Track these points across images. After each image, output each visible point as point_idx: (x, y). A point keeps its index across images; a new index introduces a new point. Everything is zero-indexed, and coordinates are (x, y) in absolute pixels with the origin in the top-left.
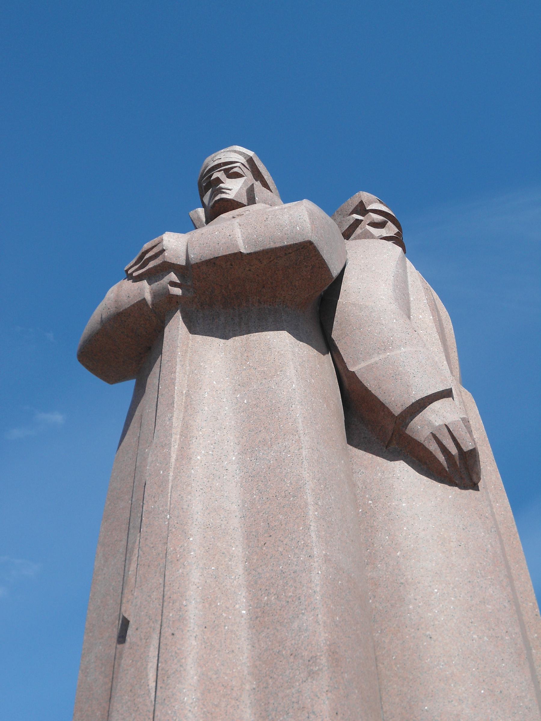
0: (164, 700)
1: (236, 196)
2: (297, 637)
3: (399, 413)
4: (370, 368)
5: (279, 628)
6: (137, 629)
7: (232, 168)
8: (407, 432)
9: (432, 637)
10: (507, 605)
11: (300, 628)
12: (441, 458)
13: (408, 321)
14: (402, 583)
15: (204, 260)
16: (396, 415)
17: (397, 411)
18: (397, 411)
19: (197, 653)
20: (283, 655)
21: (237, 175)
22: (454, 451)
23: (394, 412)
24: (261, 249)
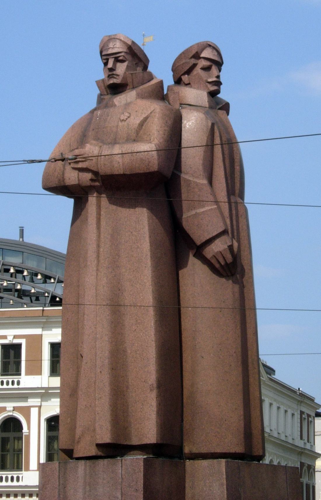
1: (122, 81)
8: (204, 253)
12: (217, 266)
17: (198, 243)
18: (198, 243)
21: (122, 61)
22: (223, 263)
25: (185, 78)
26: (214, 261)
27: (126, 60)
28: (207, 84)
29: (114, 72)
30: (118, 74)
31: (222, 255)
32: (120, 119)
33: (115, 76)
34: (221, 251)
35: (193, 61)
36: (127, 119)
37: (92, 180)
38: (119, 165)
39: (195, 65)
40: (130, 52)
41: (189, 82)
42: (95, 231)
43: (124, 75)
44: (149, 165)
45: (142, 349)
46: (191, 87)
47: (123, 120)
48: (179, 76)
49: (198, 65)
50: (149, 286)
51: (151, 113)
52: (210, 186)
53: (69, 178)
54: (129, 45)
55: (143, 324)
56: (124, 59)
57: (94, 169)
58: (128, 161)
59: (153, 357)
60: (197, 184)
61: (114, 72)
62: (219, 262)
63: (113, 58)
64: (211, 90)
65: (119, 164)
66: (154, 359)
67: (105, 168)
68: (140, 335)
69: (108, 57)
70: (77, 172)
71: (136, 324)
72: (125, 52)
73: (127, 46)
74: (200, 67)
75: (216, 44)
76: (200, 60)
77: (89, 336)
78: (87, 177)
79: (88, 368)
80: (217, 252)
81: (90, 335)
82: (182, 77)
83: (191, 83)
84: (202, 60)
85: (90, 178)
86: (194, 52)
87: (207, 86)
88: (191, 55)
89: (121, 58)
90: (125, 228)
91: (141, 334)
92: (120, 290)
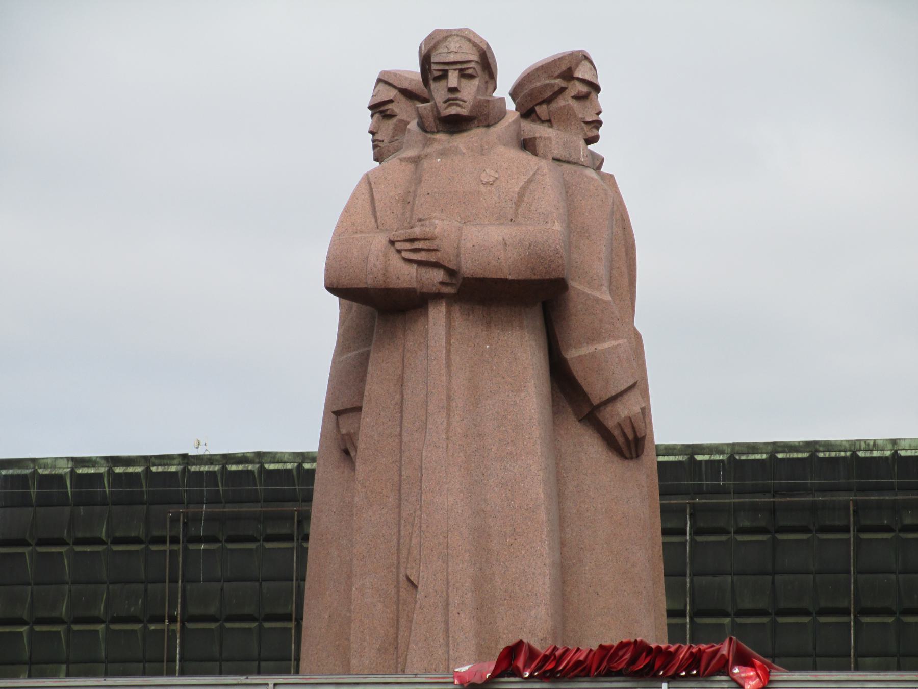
0: (457, 658)
1: (471, 111)
2: (534, 622)
3: (597, 404)
4: (581, 359)
5: (521, 611)
6: (426, 597)
7: (467, 69)
9: (599, 593)
10: (647, 565)
11: (536, 616)
12: (621, 440)
13: (638, 384)
14: (582, 548)
15: (475, 276)
16: (594, 405)
18: (596, 401)
19: (475, 629)
20: (524, 631)
21: (471, 77)
22: (631, 437)
23: (593, 402)
24: (524, 278)
25: (542, 110)
26: (616, 433)
27: (476, 75)
28: (583, 124)
29: (458, 95)
30: (465, 99)
31: (631, 421)
32: (482, 181)
33: (461, 103)
34: (630, 416)
35: (560, 83)
36: (494, 181)
37: (442, 283)
38: (500, 263)
39: (562, 90)
40: (481, 61)
41: (550, 118)
42: (444, 370)
43: (474, 101)
44: (550, 267)
45: (523, 578)
46: (551, 126)
47: (487, 183)
48: (532, 106)
49: (567, 90)
50: (536, 472)
51: (534, 174)
52: (369, 282)
53: (397, 275)
54: (483, 49)
55: (525, 535)
56: (474, 74)
57: (452, 266)
58: (515, 256)
59: (545, 592)
60: (597, 300)
61: (458, 95)
62: (624, 435)
63: (455, 70)
64: (590, 136)
65: (499, 261)
66: (548, 596)
67: (469, 267)
68: (521, 553)
69: (446, 67)
70: (415, 266)
71: (513, 534)
72: (477, 62)
73: (479, 51)
74: (573, 95)
75: (588, 51)
76: (572, 82)
77: (432, 551)
78: (438, 276)
79: (430, 606)
80: (625, 417)
81: (434, 549)
82: (537, 108)
83: (552, 119)
84: (577, 83)
85: (441, 280)
86: (564, 68)
87: (583, 128)
88: (558, 72)
89: (470, 72)
90: (492, 370)
91: (523, 552)
92: (484, 474)
